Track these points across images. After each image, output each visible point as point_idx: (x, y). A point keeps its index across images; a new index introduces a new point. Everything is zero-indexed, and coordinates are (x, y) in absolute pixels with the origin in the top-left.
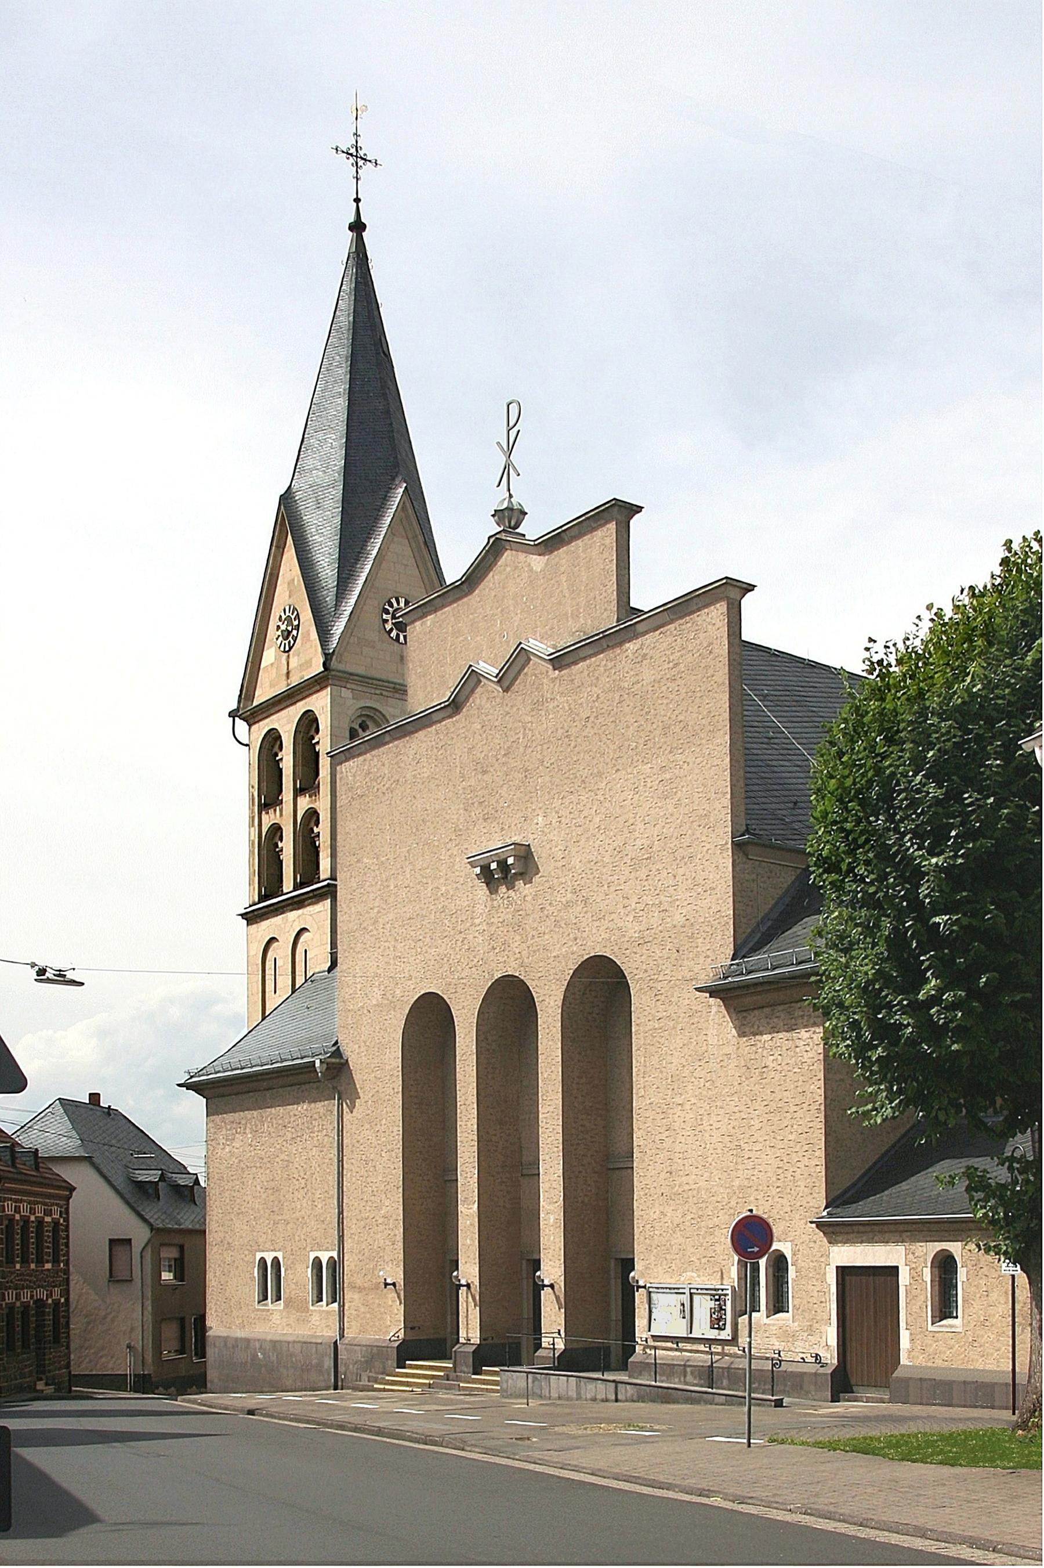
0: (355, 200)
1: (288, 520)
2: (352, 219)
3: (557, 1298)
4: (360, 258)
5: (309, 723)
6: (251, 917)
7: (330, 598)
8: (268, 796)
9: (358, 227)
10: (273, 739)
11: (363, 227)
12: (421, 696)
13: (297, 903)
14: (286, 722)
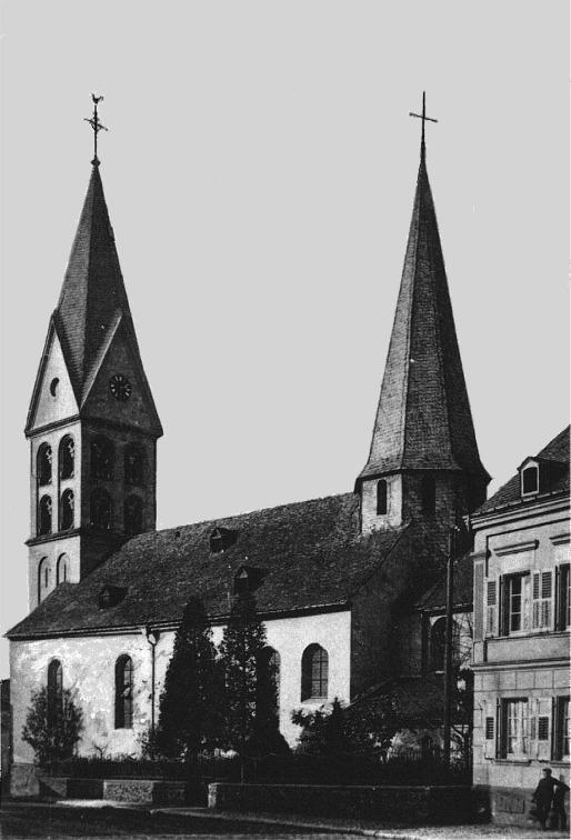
0: (93, 162)
1: (57, 325)
2: (93, 158)
3: (59, 492)
4: (96, 181)
5: (66, 442)
6: (30, 543)
7: (80, 372)
8: (43, 477)
9: (96, 162)
10: (45, 448)
11: (99, 163)
12: (565, 558)
13: (61, 536)
14: (54, 439)
